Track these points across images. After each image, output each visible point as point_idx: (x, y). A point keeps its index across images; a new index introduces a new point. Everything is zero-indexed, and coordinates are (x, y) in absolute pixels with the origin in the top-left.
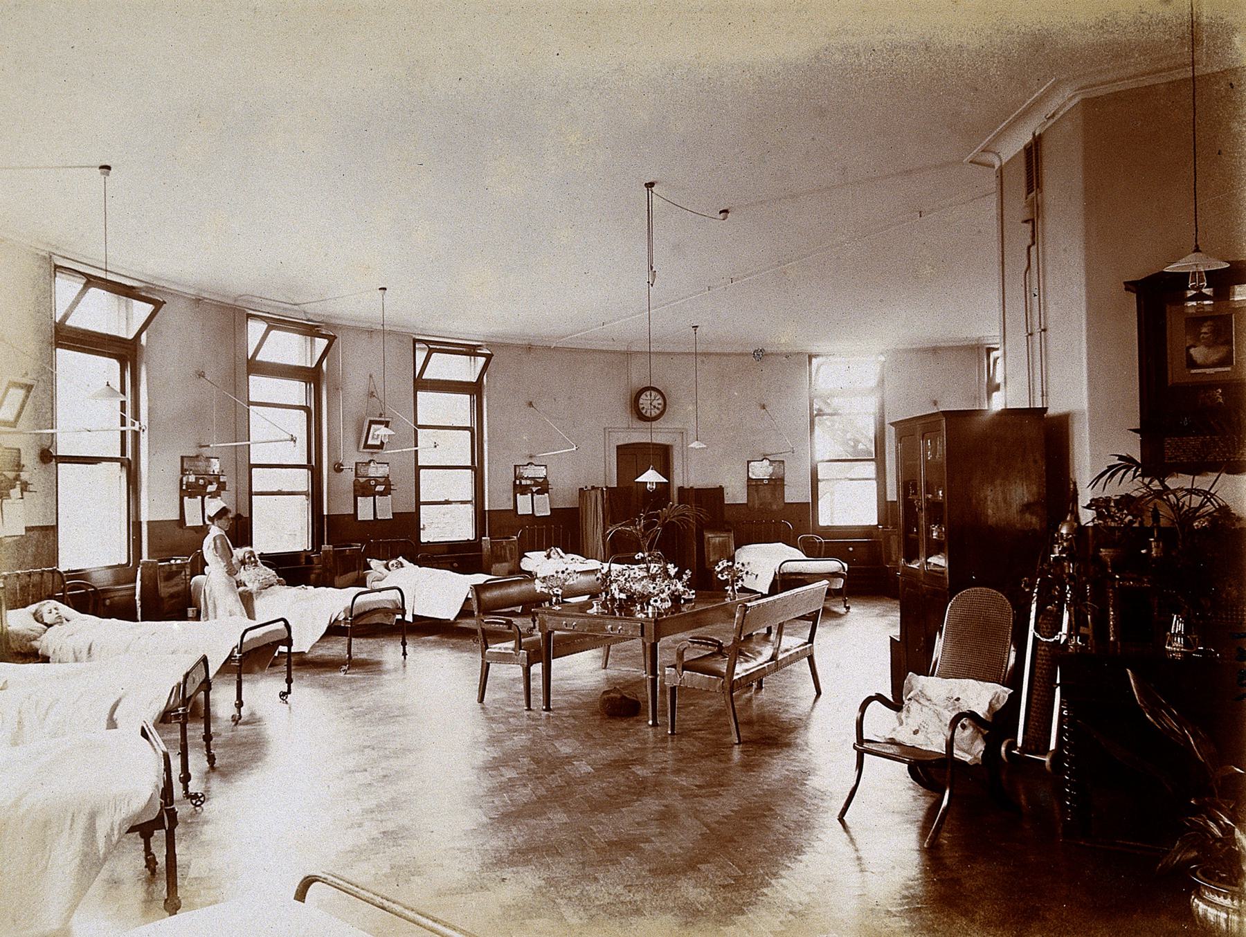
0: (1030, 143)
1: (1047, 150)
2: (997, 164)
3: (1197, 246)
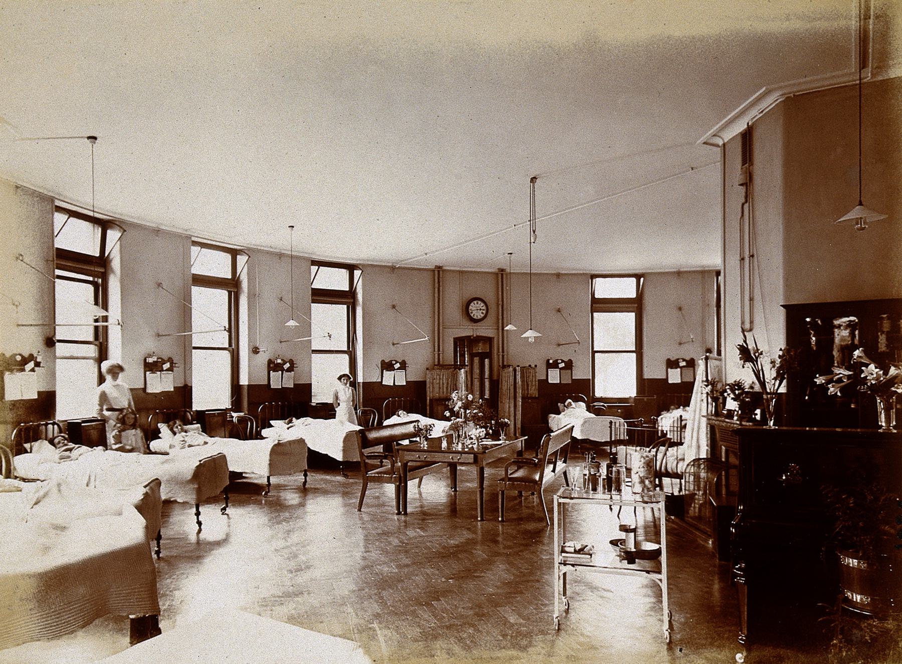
0: (745, 130)
1: (757, 135)
2: (721, 143)
3: (860, 201)
